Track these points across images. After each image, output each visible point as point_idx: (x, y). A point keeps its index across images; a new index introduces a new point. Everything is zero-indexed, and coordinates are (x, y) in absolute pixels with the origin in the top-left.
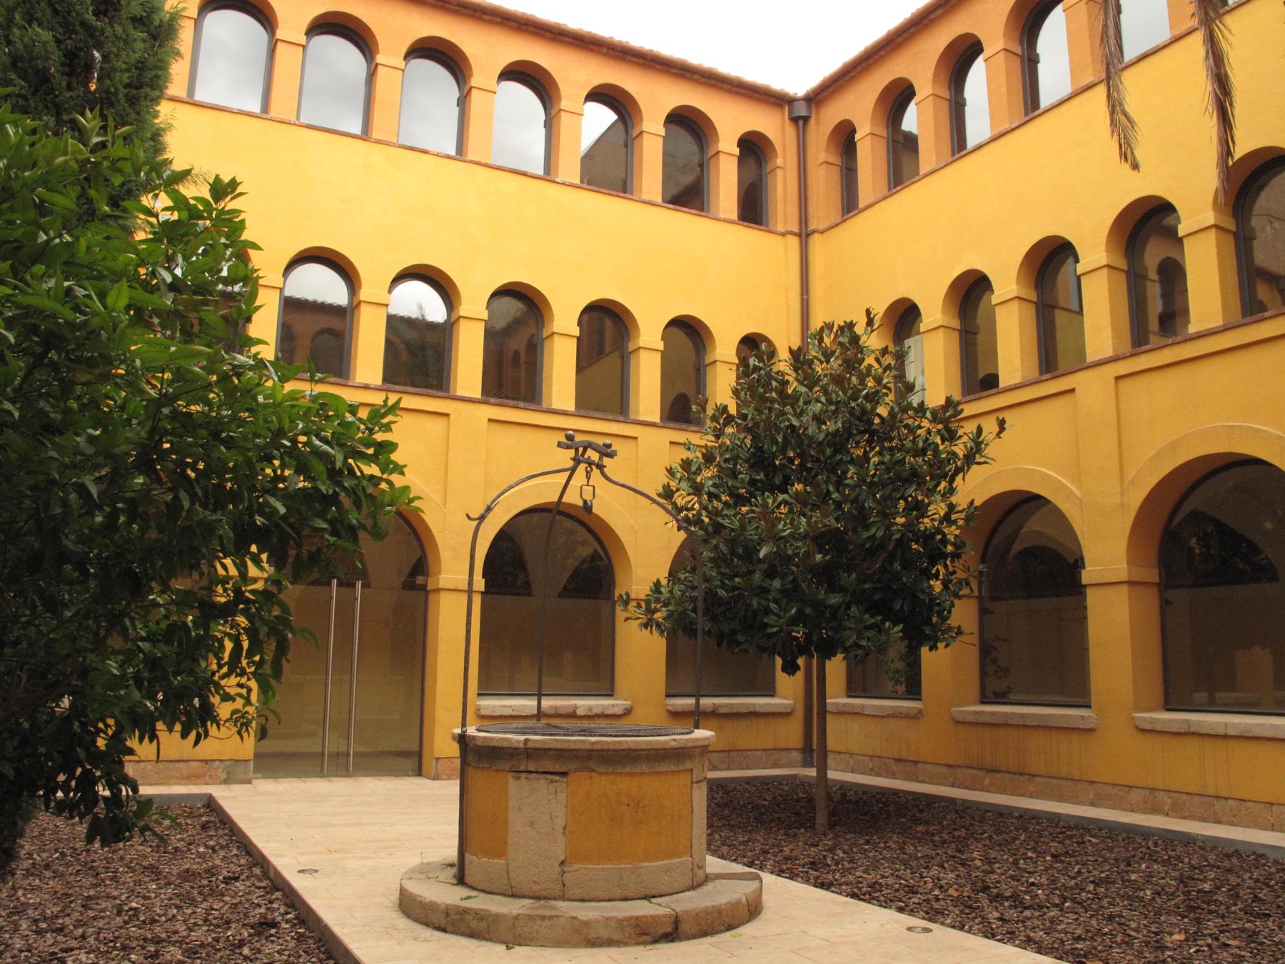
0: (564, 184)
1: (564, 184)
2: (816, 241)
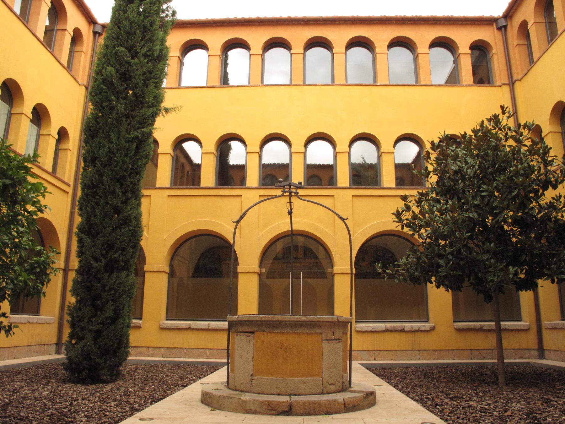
0: (381, 85)
1: (381, 85)
2: (517, 85)
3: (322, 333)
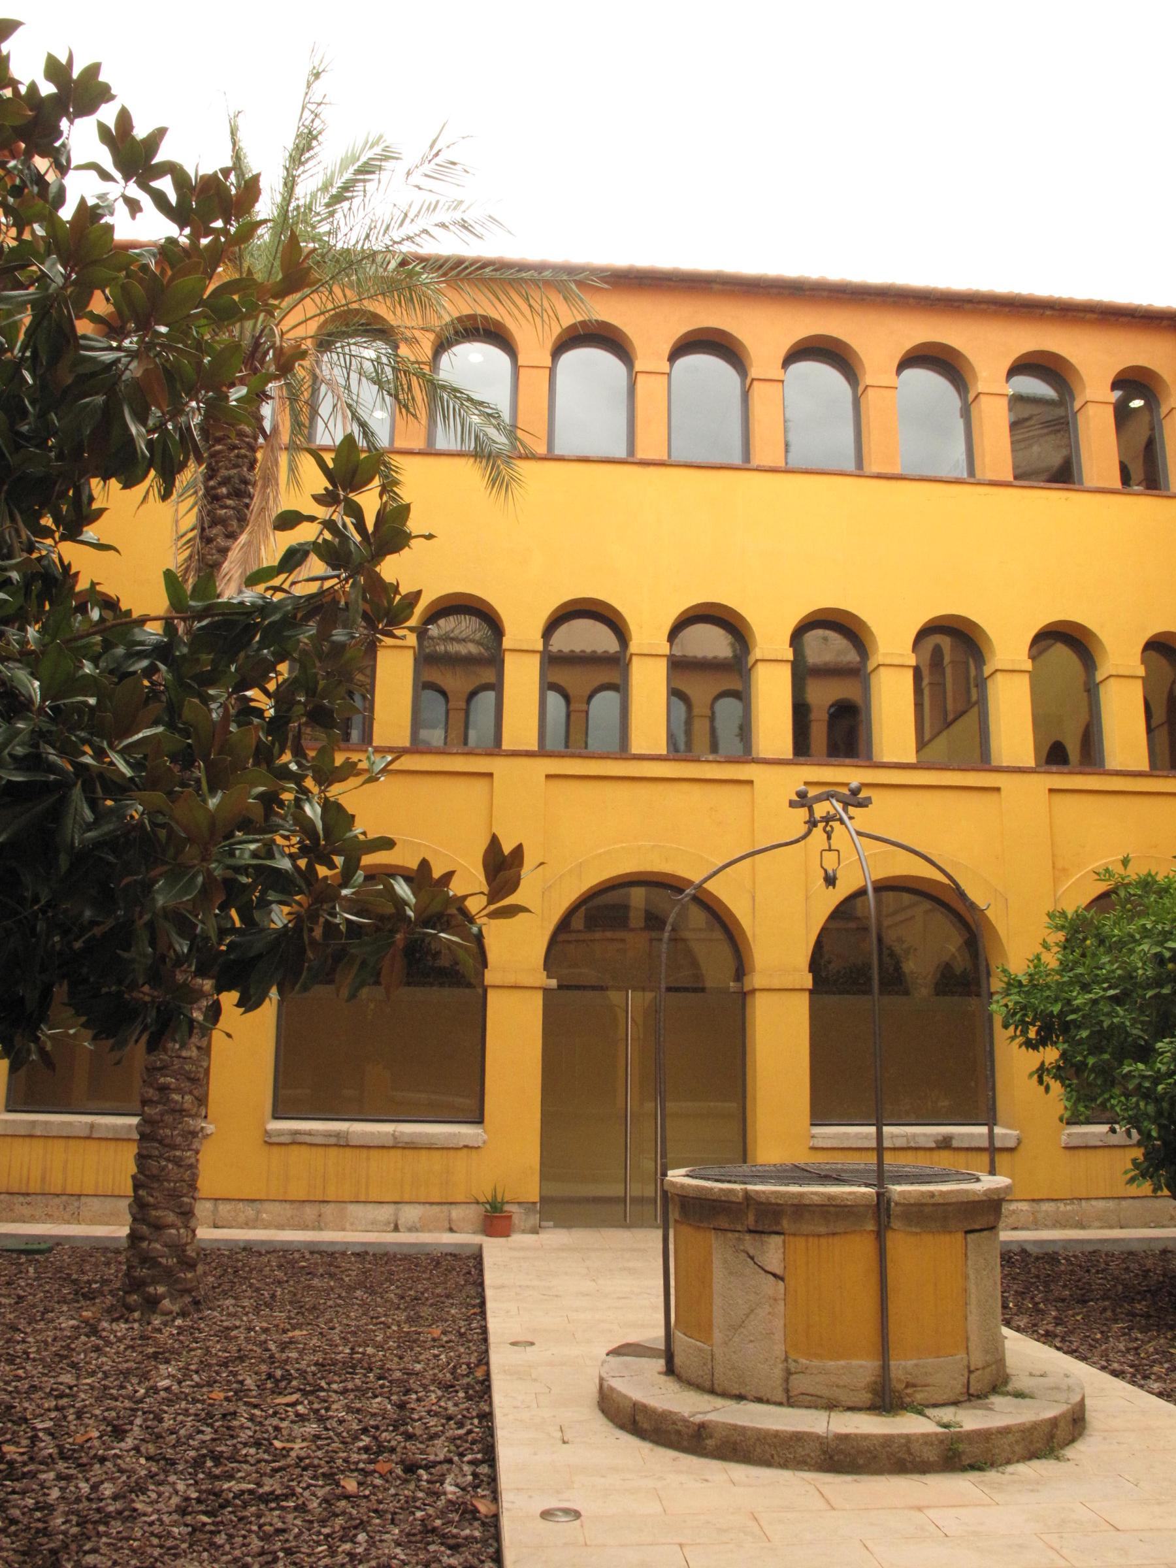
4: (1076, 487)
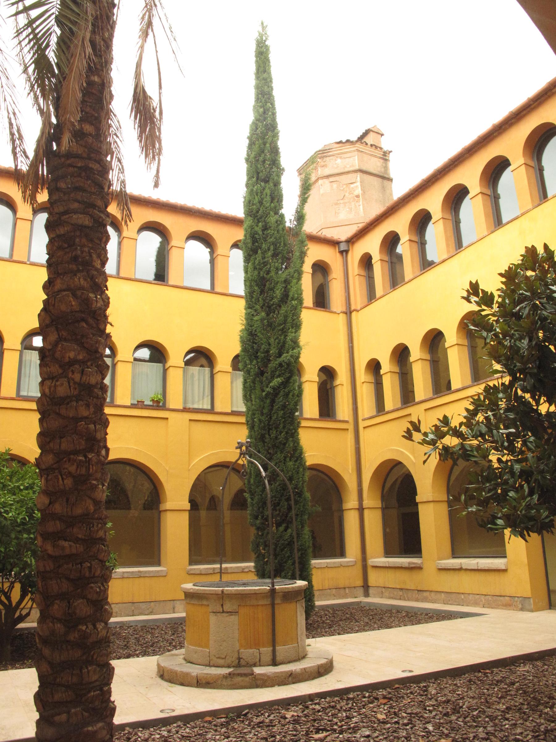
2: (354, 314)
3: (208, 605)
4: (328, 310)
